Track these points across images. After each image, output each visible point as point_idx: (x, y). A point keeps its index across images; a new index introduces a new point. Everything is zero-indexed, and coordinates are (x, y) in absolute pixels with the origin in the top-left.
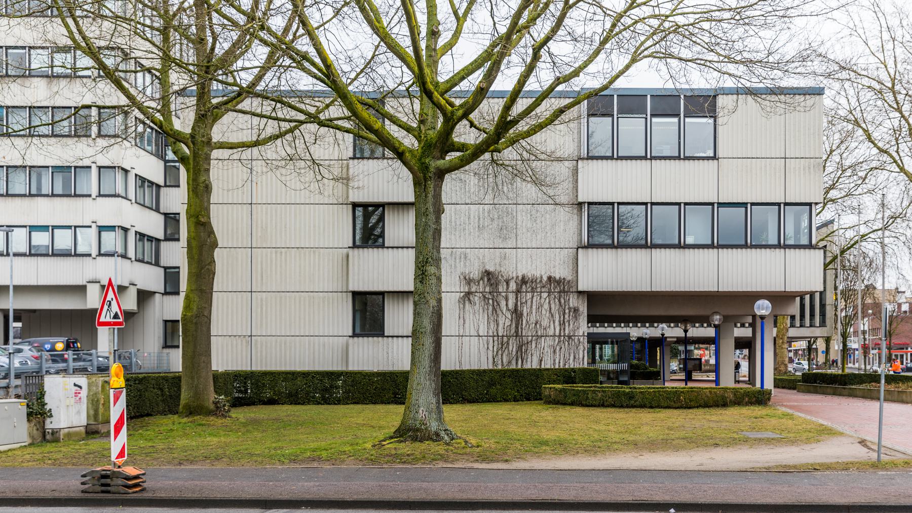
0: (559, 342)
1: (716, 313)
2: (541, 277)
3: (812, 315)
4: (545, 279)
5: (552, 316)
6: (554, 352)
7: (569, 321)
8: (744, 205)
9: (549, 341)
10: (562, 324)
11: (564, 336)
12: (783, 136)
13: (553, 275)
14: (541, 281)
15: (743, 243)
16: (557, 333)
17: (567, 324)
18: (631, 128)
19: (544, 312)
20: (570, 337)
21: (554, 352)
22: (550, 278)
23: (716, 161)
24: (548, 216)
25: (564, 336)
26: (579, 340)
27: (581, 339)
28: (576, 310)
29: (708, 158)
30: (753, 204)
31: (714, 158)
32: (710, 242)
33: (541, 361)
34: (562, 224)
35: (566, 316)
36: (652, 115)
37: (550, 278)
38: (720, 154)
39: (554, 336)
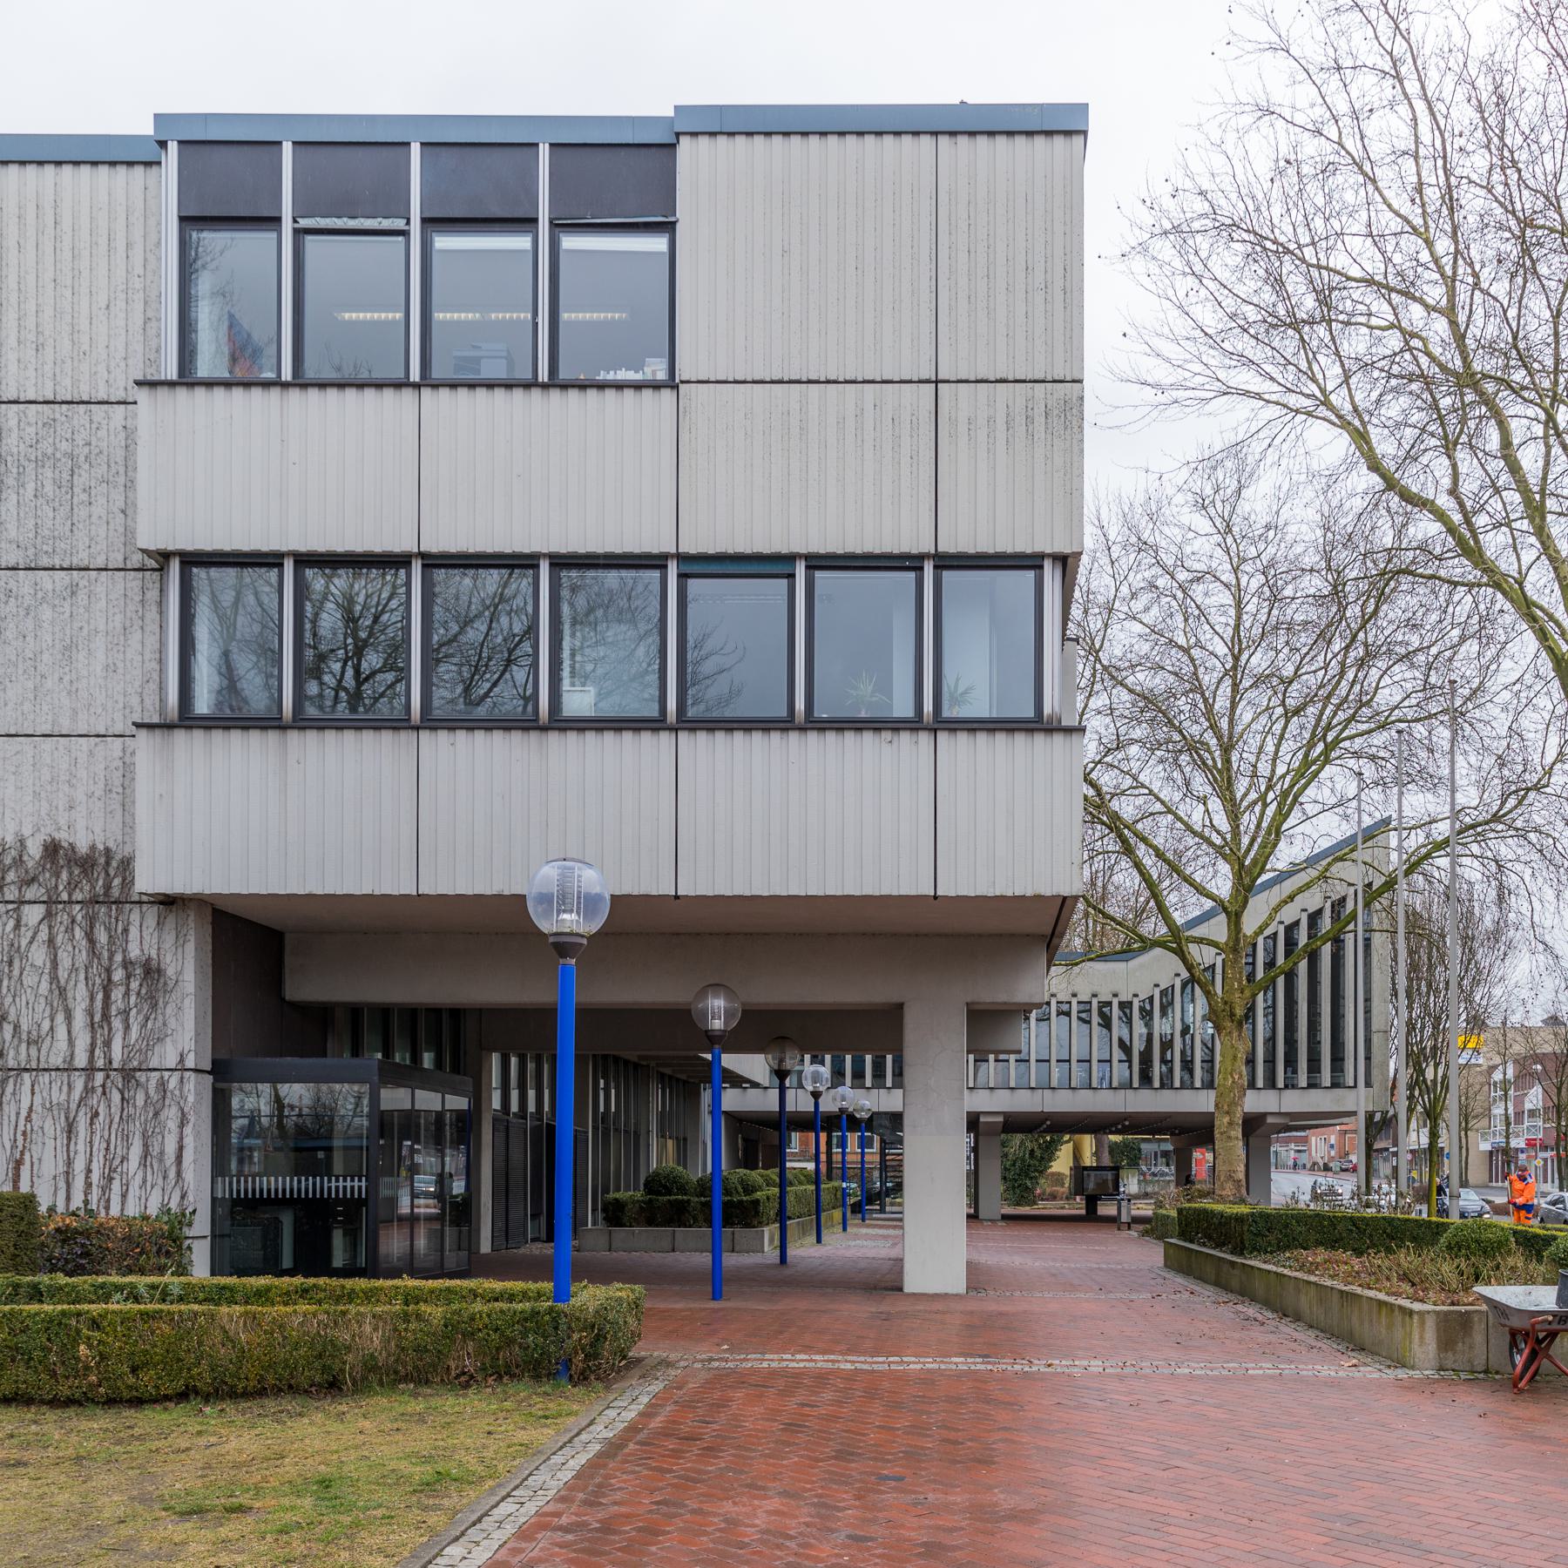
0: (89, 1090)
1: (717, 987)
2: (22, 842)
3: (1291, 1061)
4: (35, 850)
5: (62, 992)
6: (70, 1129)
7: (125, 1013)
8: (775, 565)
9: (54, 1090)
10: (100, 1022)
11: (107, 1069)
12: (926, 296)
13: (63, 836)
14: (19, 861)
15: (783, 713)
16: (81, 1060)
17: (117, 1024)
18: (360, 282)
19: (30, 979)
20: (128, 1074)
21: (70, 1129)
22: (52, 849)
23: (667, 395)
24: (46, 613)
25: (107, 1069)
26: (162, 1085)
27: (173, 1082)
28: (152, 971)
29: (656, 386)
30: (817, 562)
31: (672, 384)
32: (783, 713)
33: (19, 1163)
34: (99, 643)
35: (117, 994)
36: (433, 223)
37: (52, 849)
38: (683, 372)
39: (69, 1069)
